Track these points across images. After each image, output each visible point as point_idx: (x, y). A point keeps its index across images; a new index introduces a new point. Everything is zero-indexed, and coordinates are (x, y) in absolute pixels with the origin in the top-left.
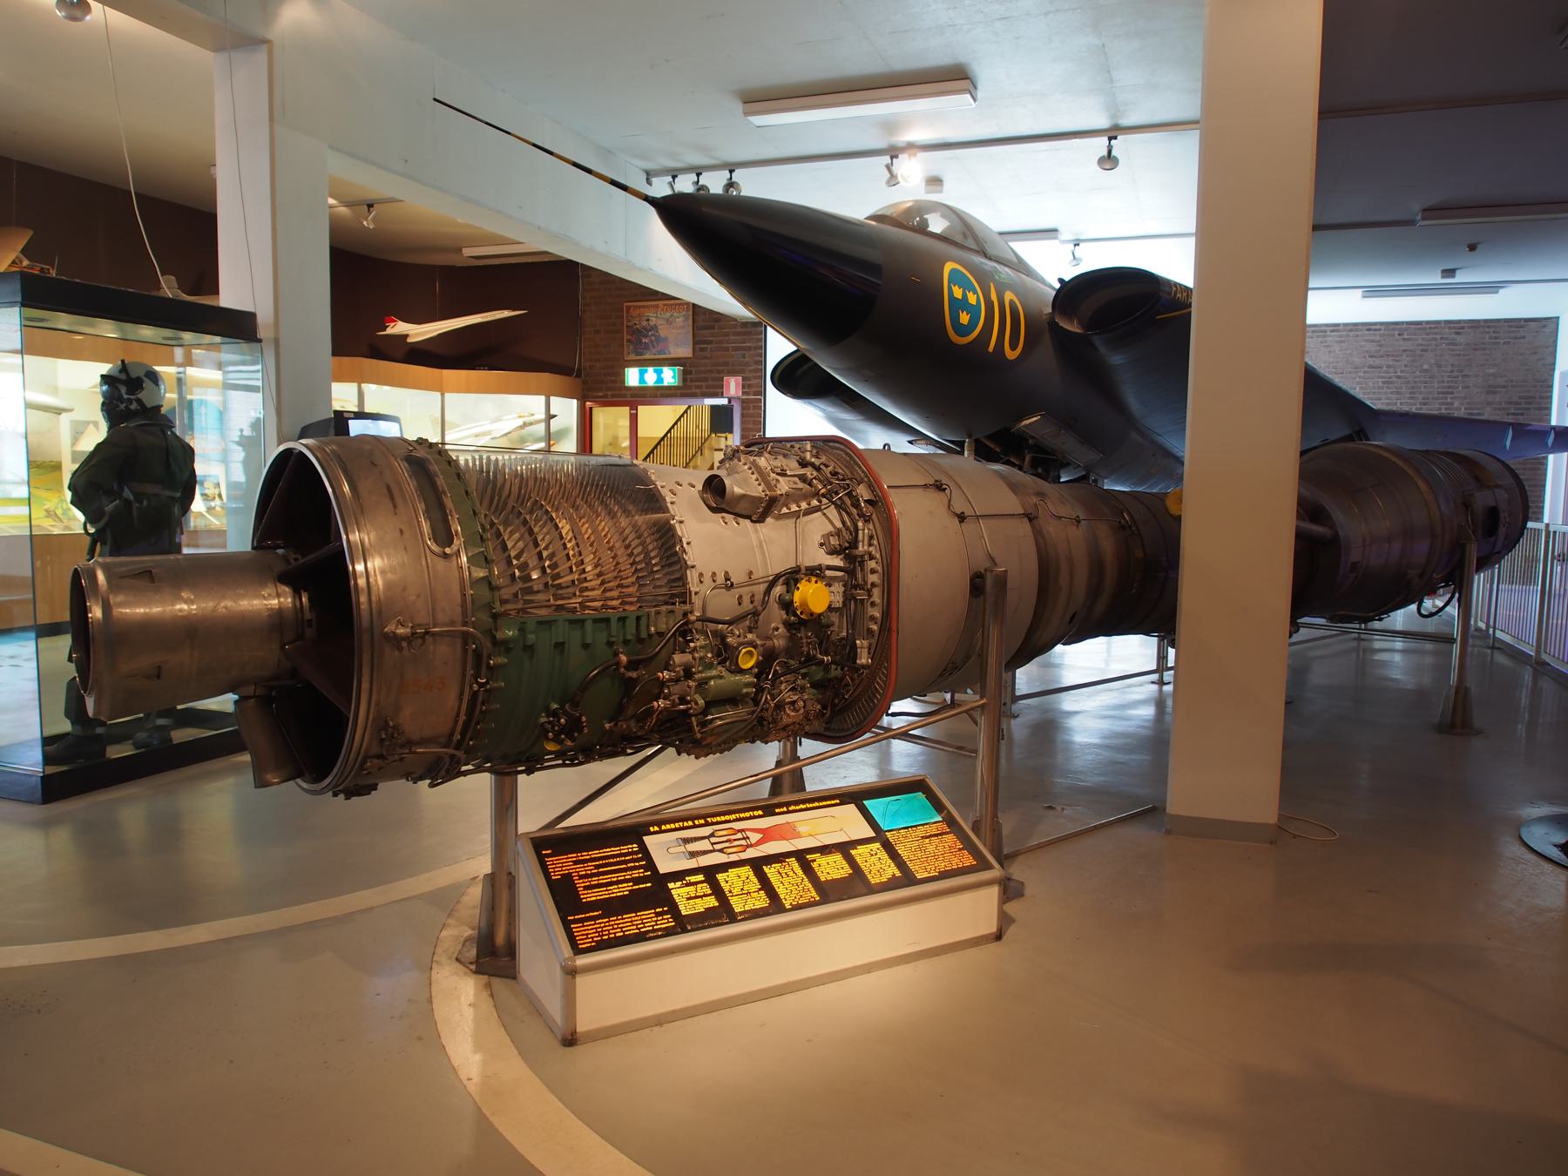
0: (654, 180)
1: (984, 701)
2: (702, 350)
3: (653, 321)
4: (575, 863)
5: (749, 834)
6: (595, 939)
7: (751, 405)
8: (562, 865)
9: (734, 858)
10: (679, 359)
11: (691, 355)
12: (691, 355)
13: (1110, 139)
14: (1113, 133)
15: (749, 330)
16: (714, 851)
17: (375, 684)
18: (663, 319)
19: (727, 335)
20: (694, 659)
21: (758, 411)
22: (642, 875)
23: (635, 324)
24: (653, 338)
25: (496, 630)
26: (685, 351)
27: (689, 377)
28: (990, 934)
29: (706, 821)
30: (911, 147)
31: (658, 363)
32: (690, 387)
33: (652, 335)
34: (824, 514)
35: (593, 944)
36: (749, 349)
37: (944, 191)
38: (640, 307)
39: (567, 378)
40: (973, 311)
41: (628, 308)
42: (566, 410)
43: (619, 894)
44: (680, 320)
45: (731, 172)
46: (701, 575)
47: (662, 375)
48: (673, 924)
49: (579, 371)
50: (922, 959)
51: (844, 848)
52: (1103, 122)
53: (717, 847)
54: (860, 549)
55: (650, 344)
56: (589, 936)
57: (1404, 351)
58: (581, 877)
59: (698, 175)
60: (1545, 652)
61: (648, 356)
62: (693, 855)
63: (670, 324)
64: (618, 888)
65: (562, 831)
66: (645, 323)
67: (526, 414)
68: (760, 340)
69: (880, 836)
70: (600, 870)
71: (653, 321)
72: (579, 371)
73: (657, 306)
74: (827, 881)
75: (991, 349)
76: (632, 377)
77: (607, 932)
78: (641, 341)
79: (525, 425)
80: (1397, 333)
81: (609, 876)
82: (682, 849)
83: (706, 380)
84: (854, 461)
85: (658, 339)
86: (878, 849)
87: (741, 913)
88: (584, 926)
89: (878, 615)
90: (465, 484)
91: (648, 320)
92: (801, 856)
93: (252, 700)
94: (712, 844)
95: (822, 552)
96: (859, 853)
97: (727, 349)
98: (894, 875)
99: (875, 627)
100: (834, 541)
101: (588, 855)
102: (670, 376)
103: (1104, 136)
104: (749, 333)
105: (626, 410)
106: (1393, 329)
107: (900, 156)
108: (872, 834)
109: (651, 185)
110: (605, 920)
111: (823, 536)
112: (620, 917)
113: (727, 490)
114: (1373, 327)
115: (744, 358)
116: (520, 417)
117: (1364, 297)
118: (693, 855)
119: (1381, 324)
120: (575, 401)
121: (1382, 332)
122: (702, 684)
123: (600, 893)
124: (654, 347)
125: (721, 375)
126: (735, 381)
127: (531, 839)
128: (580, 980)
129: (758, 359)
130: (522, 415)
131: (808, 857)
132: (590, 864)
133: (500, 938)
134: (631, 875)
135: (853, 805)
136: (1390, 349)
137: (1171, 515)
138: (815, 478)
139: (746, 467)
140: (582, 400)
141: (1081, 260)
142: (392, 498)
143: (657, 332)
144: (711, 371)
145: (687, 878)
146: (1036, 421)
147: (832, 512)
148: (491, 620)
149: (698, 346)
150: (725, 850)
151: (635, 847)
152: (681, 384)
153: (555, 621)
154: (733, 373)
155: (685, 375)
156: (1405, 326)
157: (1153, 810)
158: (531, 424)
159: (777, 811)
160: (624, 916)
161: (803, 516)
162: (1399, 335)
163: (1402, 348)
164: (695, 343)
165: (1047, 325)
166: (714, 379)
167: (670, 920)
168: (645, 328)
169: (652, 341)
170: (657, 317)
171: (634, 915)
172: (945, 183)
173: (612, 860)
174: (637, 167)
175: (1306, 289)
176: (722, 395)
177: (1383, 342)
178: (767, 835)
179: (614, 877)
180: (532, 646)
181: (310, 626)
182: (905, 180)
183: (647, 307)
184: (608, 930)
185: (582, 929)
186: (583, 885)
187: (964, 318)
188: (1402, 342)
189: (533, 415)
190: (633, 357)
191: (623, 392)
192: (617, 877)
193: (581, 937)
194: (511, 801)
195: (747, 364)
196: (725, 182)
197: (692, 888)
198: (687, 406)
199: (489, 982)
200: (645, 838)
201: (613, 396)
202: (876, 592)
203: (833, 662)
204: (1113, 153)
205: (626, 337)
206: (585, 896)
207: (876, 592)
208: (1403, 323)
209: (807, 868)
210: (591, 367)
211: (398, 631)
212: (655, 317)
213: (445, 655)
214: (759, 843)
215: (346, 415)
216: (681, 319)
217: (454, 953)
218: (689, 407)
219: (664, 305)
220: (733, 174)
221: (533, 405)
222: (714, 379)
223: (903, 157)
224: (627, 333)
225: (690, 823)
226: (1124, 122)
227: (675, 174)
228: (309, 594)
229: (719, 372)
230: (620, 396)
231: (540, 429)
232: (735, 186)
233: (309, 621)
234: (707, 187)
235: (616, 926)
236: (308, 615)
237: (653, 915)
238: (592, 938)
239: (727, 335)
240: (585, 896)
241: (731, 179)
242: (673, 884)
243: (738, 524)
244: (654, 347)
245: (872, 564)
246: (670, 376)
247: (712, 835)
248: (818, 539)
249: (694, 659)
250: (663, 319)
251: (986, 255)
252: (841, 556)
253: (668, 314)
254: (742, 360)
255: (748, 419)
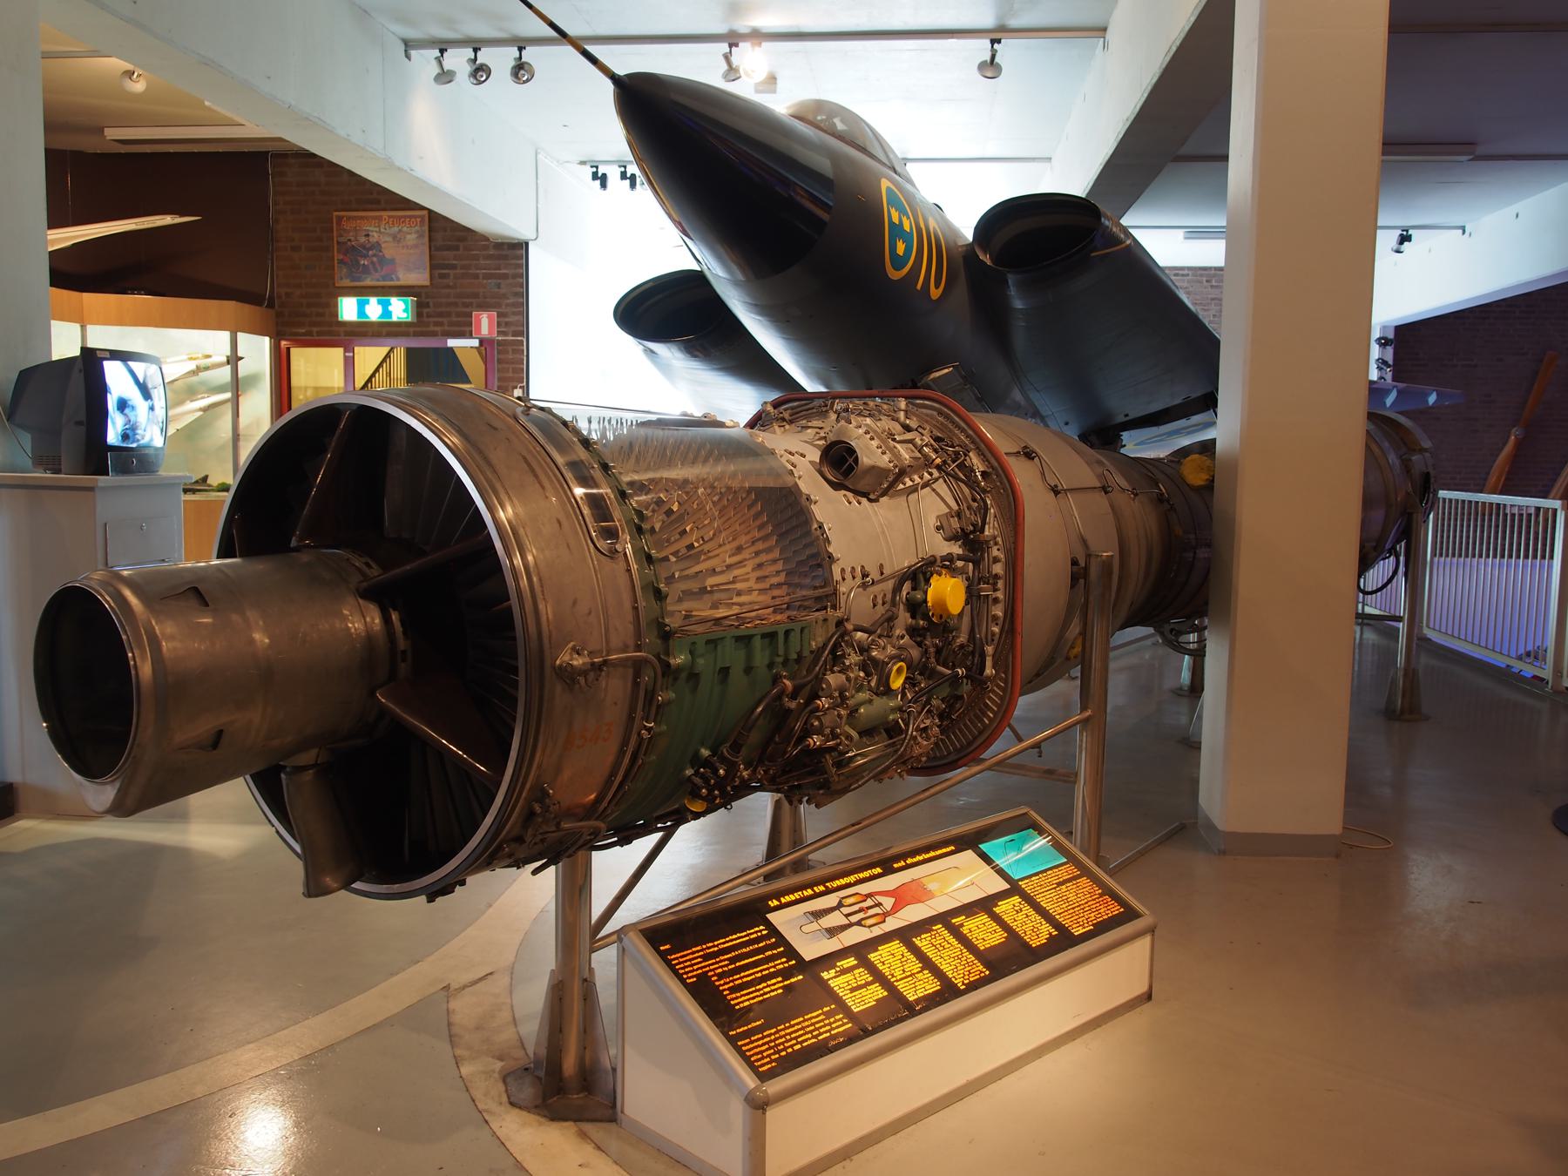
0: (413, 53)
1: (1088, 713)
2: (442, 276)
3: (375, 237)
4: (706, 957)
5: (880, 899)
6: (773, 1057)
7: (510, 349)
8: (692, 959)
9: (877, 931)
10: (413, 287)
11: (427, 283)
12: (427, 283)
13: (993, 42)
14: (996, 36)
15: (504, 253)
16: (851, 925)
17: (541, 738)
18: (389, 235)
19: (476, 258)
20: (848, 679)
21: (518, 356)
22: (786, 965)
23: (350, 240)
24: (375, 259)
25: (668, 654)
26: (419, 277)
27: (425, 311)
28: (1142, 994)
29: (826, 887)
30: (758, 36)
31: (384, 291)
32: (428, 325)
33: (374, 255)
34: (934, 490)
35: (773, 1064)
36: (505, 276)
37: (778, 90)
38: (355, 218)
39: (258, 308)
40: (907, 238)
41: (340, 219)
42: (257, 351)
43: (772, 994)
44: (411, 238)
45: (520, 49)
46: (843, 570)
47: (390, 308)
48: (850, 1025)
49: (271, 299)
50: (1079, 1037)
51: (985, 905)
52: (987, 20)
53: (854, 919)
54: (987, 533)
55: (371, 266)
56: (765, 1054)
57: (1212, 299)
58: (720, 976)
59: (476, 50)
60: (1428, 626)
61: (368, 282)
62: (832, 932)
63: (399, 241)
64: (768, 986)
65: (672, 918)
66: (363, 239)
67: (200, 356)
68: (520, 266)
69: (1014, 889)
70: (738, 964)
71: (375, 237)
72: (271, 299)
73: (380, 218)
74: (986, 949)
75: (919, 287)
76: (348, 308)
77: (782, 1047)
78: (358, 262)
79: (199, 370)
80: (1205, 279)
81: (751, 971)
82: (814, 926)
83: (449, 314)
84: (953, 422)
85: (382, 260)
86: (1020, 903)
87: (918, 1001)
88: (752, 1042)
89: (1000, 614)
90: (598, 454)
91: (368, 235)
92: (944, 918)
93: (311, 771)
94: (847, 916)
95: (939, 537)
96: (1004, 908)
97: (476, 277)
98: (1050, 934)
99: (996, 629)
100: (955, 523)
101: (714, 946)
102: (400, 309)
103: (986, 38)
104: (506, 257)
105: (338, 353)
106: (1201, 275)
107: (740, 44)
108: (1005, 886)
109: (410, 60)
110: (773, 1031)
111: (938, 517)
112: (787, 1025)
113: (860, 460)
114: (1181, 272)
115: (499, 288)
116: (191, 359)
117: (1186, 238)
118: (832, 932)
119: (1189, 268)
120: (267, 339)
121: (1190, 277)
122: (853, 711)
123: (752, 996)
124: (376, 271)
125: (468, 310)
126: (489, 317)
127: (641, 931)
128: (772, 1114)
129: (519, 289)
130: (194, 356)
131: (953, 921)
132: (722, 958)
133: (569, 1065)
134: (774, 967)
135: (970, 851)
136: (1198, 297)
137: (1188, 485)
138: (926, 445)
139: (861, 431)
140: (277, 337)
141: (593, 179)
142: (536, 476)
143: (381, 251)
144: (456, 304)
145: (838, 964)
146: (947, 373)
147: (941, 486)
148: (659, 641)
149: (437, 272)
150: (863, 922)
151: (762, 930)
152: (415, 321)
153: (722, 638)
154: (484, 307)
155: (420, 308)
156: (1213, 272)
157: (1182, 828)
158: (207, 368)
159: (895, 866)
160: (792, 1023)
161: (922, 489)
162: (1207, 281)
163: (1210, 296)
164: (433, 267)
165: (961, 260)
166: (458, 315)
167: (845, 1021)
168: (363, 246)
169: (373, 263)
170: (380, 232)
171: (801, 1019)
172: (778, 81)
173: (744, 950)
174: (393, 33)
175: (1376, 228)
176: (471, 334)
177: (1191, 289)
178: (901, 898)
179: (756, 972)
180: (698, 674)
181: (404, 660)
182: (747, 75)
183: (366, 218)
184: (783, 1043)
185: (751, 1046)
186: (726, 987)
187: (901, 248)
188: (1210, 289)
189: (209, 356)
190: (347, 282)
191: (334, 328)
192: (761, 971)
193: (755, 1057)
194: (585, 880)
195: (504, 296)
196: (513, 63)
197: (848, 977)
198: (389, 348)
199: (581, 1130)
200: (769, 916)
201: (319, 334)
202: (1000, 584)
203: (967, 677)
204: (997, 60)
205: (337, 256)
206: (736, 1001)
207: (1000, 584)
208: (1210, 268)
209: (956, 932)
210: (287, 294)
211: (575, 663)
212: (379, 231)
213: (615, 689)
214: (896, 908)
215: (99, 354)
216: (414, 236)
217: (500, 1096)
218: (392, 350)
219: (389, 217)
220: (524, 52)
221: (215, 343)
222: (458, 315)
223: (744, 46)
224: (338, 252)
225: (810, 892)
226: (1014, 23)
227: (444, 47)
228: (400, 614)
229: (466, 305)
230: (330, 333)
231: (225, 374)
232: (526, 67)
233: (404, 652)
234: (486, 66)
235: (788, 1037)
236: (402, 644)
237: (822, 1017)
238: (769, 1056)
239: (476, 258)
240: (736, 1001)
241: (520, 58)
242: (826, 973)
243: (860, 503)
244: (376, 271)
245: (995, 552)
246: (400, 309)
247: (840, 905)
248: (932, 522)
249: (848, 679)
250: (389, 235)
251: (895, 172)
252: (960, 543)
253: (396, 229)
254: (497, 290)
255: (507, 366)
